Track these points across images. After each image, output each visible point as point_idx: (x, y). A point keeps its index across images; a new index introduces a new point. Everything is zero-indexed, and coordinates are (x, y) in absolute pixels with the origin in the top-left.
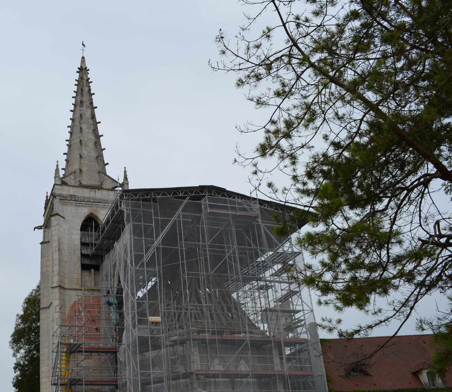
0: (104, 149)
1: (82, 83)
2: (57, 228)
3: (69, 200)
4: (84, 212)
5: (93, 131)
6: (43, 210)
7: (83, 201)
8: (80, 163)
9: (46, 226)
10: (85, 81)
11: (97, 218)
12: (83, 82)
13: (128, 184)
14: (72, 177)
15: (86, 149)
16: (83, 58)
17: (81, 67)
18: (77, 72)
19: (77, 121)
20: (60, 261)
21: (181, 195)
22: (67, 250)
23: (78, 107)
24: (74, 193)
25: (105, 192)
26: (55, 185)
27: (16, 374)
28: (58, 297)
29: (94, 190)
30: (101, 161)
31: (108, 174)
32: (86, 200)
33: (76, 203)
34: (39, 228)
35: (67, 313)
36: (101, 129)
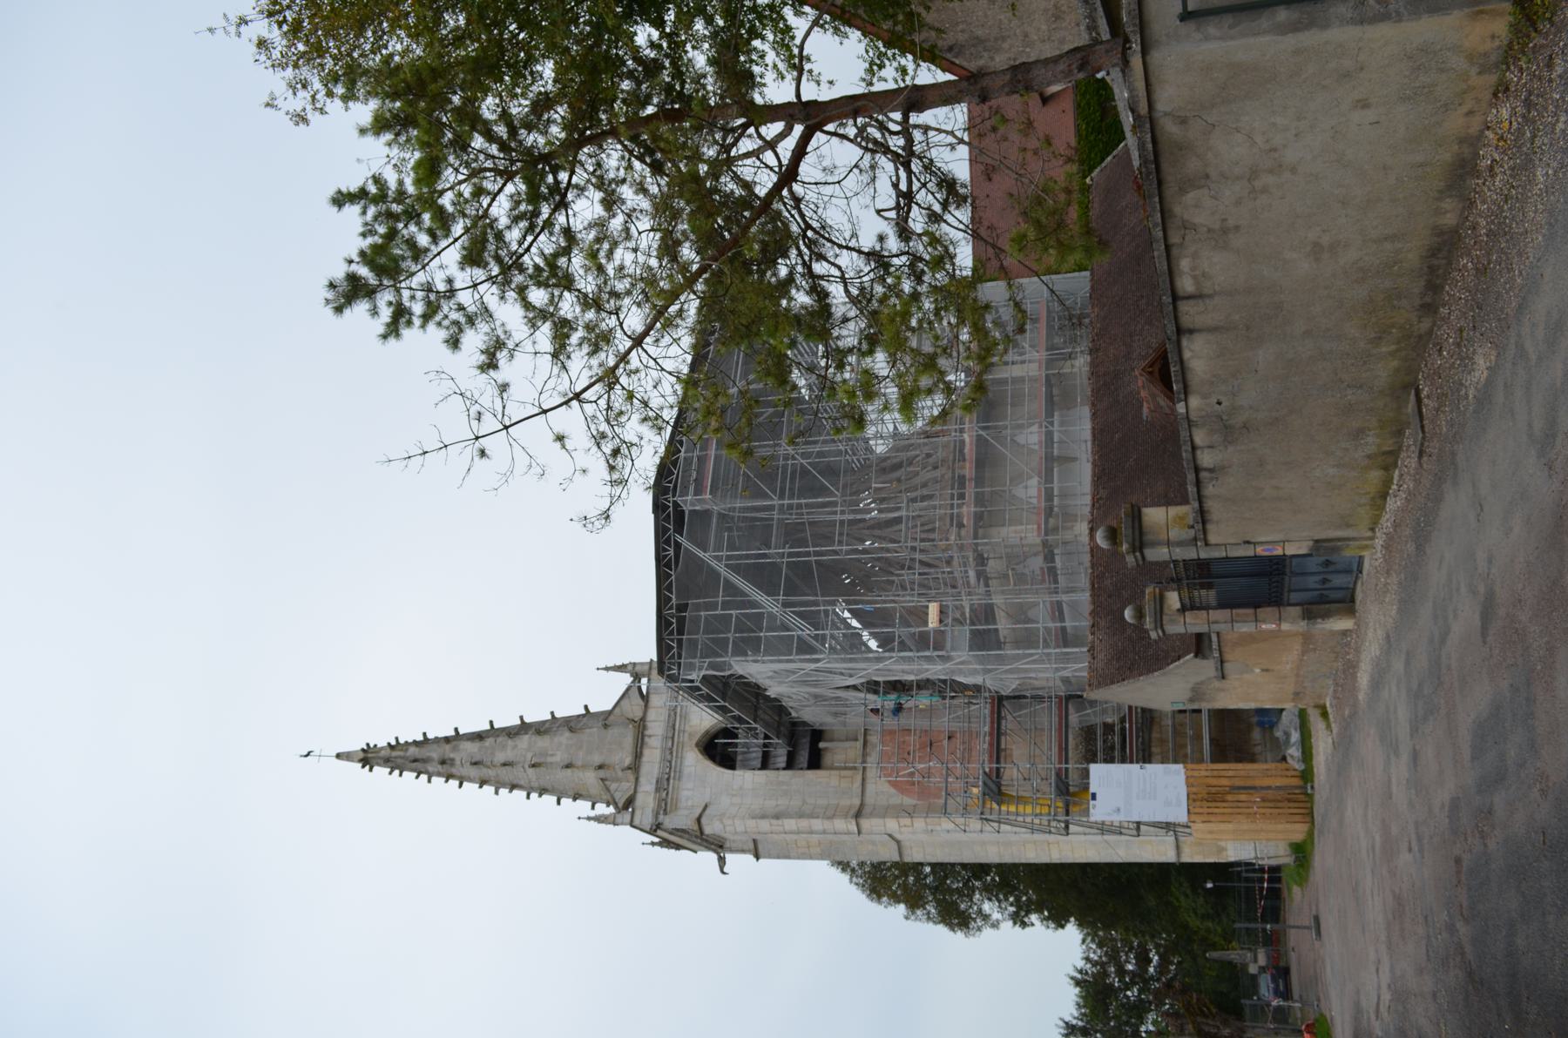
0: (552, 713)
1: (399, 761)
3: (667, 794)
4: (694, 761)
7: (670, 762)
8: (584, 767)
9: (718, 846)
10: (395, 754)
11: (707, 732)
12: (396, 757)
13: (634, 664)
14: (613, 786)
15: (552, 755)
16: (338, 756)
17: (360, 761)
18: (371, 770)
20: (801, 815)
22: (777, 799)
23: (454, 771)
24: (651, 784)
29: (646, 739)
30: (580, 722)
31: (609, 707)
32: (669, 757)
34: (722, 861)
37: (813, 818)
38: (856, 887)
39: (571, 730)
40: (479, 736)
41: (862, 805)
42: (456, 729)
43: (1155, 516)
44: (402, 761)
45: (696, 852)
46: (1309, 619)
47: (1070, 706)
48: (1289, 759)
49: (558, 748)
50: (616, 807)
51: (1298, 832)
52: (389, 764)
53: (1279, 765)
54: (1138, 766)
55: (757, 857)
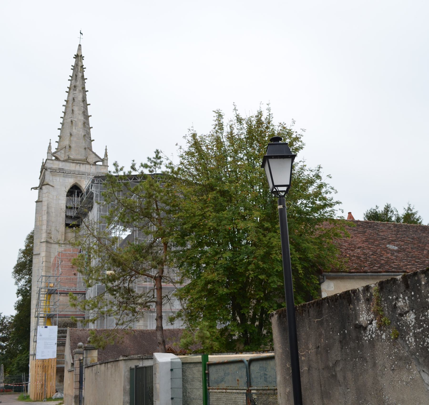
0: (92, 127)
1: (77, 69)
2: (46, 196)
3: (58, 172)
4: (70, 182)
5: (83, 112)
6: (40, 174)
7: (70, 173)
8: (70, 140)
9: (40, 188)
10: (79, 67)
11: (81, 187)
12: (78, 68)
13: (107, 160)
14: (63, 151)
15: (75, 128)
16: (80, 45)
17: (77, 54)
18: (74, 58)
19: (71, 102)
20: (48, 221)
21: (139, 180)
22: (54, 212)
23: (72, 90)
24: (62, 166)
25: (88, 166)
26: (47, 160)
27: (17, 299)
28: (45, 250)
29: (79, 165)
30: (88, 138)
31: (93, 150)
32: (72, 173)
33: (64, 175)
34: (36, 188)
35: (52, 261)
36: (90, 110)
37: (47, 226)
38: (33, 230)
39: (85, 136)
40: (84, 100)
41: (51, 243)
42: (88, 91)
43: (95, 353)
44: (77, 71)
45: (39, 179)
46: (75, 397)
47: (82, 318)
48: (57, 393)
49: (78, 131)
50: (55, 153)
51: (32, 397)
52: (76, 66)
53: (55, 390)
54: (56, 342)
55: (36, 202)
